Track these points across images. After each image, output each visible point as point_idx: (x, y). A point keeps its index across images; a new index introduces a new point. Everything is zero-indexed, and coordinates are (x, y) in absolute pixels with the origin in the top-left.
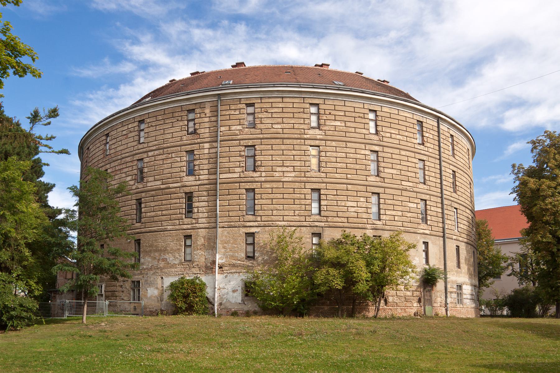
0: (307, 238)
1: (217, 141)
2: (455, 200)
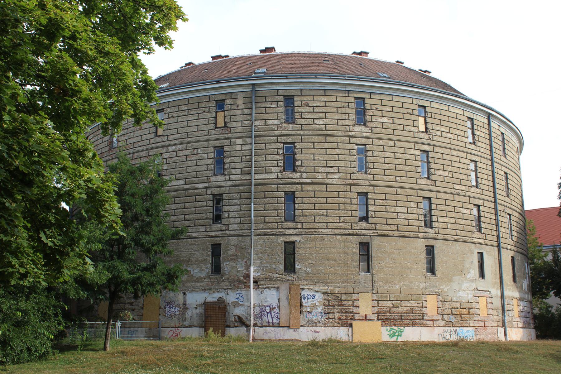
0: (353, 248)
1: (251, 137)
2: (509, 205)
